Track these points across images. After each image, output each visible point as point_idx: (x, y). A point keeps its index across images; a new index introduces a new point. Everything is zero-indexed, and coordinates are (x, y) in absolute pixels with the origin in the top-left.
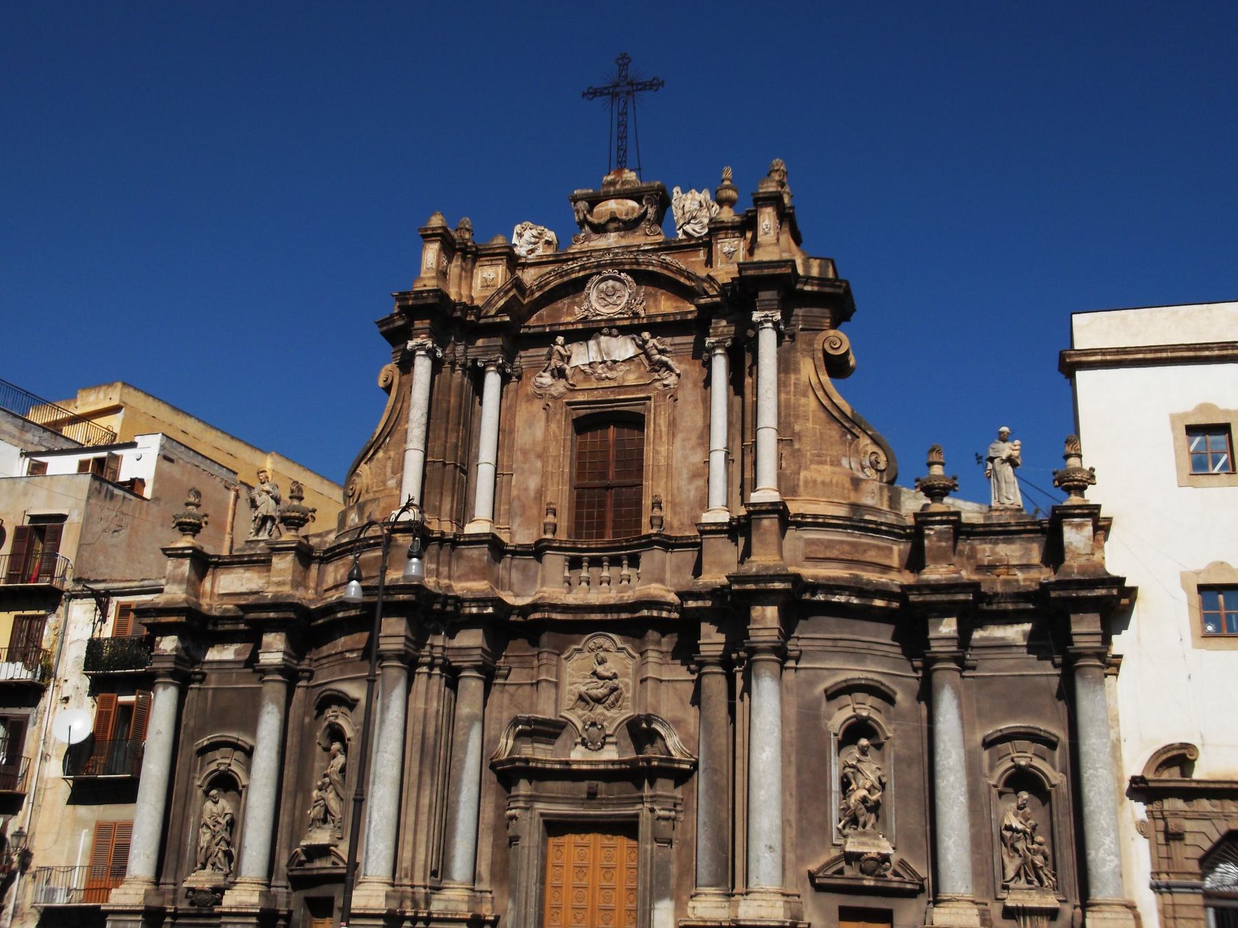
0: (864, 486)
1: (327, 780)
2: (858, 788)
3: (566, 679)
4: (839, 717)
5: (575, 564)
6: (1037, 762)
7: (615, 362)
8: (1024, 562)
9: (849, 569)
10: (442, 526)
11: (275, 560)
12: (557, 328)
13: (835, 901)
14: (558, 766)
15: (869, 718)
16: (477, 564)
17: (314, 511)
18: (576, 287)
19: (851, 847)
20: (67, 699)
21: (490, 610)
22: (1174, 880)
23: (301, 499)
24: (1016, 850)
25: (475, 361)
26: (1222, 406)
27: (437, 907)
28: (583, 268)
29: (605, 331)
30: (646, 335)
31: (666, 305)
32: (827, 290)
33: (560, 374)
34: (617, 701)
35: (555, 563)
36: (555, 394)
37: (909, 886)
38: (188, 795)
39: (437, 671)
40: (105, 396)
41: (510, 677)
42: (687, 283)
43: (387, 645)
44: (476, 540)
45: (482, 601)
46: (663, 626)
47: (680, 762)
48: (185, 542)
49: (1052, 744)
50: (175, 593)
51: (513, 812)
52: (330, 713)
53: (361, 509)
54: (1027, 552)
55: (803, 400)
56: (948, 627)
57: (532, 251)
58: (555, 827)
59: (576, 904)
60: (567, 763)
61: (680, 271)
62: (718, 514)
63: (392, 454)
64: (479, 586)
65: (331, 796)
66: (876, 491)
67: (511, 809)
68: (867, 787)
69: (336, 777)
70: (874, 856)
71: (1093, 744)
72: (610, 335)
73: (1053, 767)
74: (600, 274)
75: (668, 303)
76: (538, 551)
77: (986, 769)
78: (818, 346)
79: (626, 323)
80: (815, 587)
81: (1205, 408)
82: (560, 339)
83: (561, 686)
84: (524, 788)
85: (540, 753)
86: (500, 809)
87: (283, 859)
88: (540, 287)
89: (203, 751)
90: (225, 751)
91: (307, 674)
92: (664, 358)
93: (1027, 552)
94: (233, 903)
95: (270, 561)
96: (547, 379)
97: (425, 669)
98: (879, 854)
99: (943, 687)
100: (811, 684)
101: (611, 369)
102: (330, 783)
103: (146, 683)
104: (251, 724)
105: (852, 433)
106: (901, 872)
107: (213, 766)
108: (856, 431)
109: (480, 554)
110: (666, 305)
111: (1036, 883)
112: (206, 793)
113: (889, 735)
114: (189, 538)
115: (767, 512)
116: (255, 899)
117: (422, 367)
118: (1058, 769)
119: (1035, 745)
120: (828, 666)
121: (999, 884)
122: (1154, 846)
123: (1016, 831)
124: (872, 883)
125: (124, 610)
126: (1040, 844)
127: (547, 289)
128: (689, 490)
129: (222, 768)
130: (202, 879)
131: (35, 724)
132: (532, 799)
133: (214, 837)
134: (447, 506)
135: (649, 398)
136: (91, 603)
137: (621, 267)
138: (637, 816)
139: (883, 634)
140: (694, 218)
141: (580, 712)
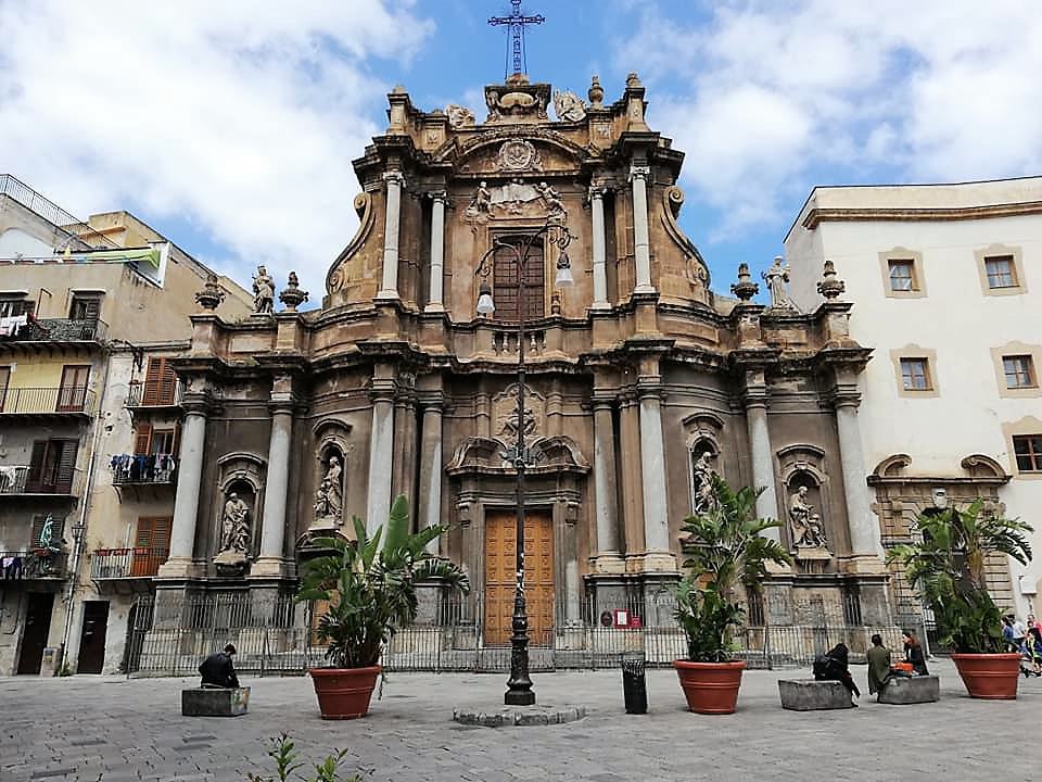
0: (696, 288)
1: (329, 483)
3: (496, 415)
4: (692, 439)
5: (499, 337)
6: (811, 468)
7: (521, 202)
8: (797, 341)
10: (411, 305)
11: (280, 326)
15: (708, 439)
17: (307, 293)
18: (493, 149)
20: (110, 428)
21: (448, 365)
22: (896, 540)
23: (297, 285)
25: (426, 194)
26: (909, 248)
28: (498, 136)
29: (515, 180)
30: (544, 184)
31: (555, 166)
32: (672, 158)
33: (483, 208)
35: (486, 337)
36: (481, 222)
38: (214, 497)
40: (112, 221)
41: (456, 413)
42: (572, 151)
43: (276, 397)
44: (434, 317)
46: (564, 380)
47: (581, 468)
48: (207, 312)
49: (819, 456)
50: (202, 349)
51: (464, 504)
52: (328, 438)
53: (345, 293)
54: (798, 336)
55: (658, 231)
56: (759, 381)
57: (459, 124)
58: (492, 513)
60: (502, 470)
61: (566, 143)
62: (601, 303)
65: (331, 495)
72: (518, 183)
74: (510, 140)
76: (473, 328)
80: (677, 351)
81: (898, 250)
82: (484, 184)
84: (470, 487)
85: (481, 464)
86: (453, 503)
88: (468, 148)
89: (225, 466)
90: (242, 465)
91: (305, 410)
92: (557, 201)
93: (798, 336)
96: (474, 211)
101: (519, 207)
103: (179, 415)
105: (688, 255)
107: (233, 476)
109: (438, 327)
110: (555, 166)
111: (814, 544)
112: (227, 495)
113: (720, 450)
115: (648, 300)
116: (277, 569)
117: (394, 192)
119: (809, 457)
122: (882, 519)
123: (802, 511)
125: (155, 363)
126: (817, 519)
128: (575, 290)
129: (240, 477)
130: (229, 557)
131: (84, 446)
132: (476, 495)
136: (130, 358)
138: (552, 505)
139: (711, 388)
141: (507, 437)
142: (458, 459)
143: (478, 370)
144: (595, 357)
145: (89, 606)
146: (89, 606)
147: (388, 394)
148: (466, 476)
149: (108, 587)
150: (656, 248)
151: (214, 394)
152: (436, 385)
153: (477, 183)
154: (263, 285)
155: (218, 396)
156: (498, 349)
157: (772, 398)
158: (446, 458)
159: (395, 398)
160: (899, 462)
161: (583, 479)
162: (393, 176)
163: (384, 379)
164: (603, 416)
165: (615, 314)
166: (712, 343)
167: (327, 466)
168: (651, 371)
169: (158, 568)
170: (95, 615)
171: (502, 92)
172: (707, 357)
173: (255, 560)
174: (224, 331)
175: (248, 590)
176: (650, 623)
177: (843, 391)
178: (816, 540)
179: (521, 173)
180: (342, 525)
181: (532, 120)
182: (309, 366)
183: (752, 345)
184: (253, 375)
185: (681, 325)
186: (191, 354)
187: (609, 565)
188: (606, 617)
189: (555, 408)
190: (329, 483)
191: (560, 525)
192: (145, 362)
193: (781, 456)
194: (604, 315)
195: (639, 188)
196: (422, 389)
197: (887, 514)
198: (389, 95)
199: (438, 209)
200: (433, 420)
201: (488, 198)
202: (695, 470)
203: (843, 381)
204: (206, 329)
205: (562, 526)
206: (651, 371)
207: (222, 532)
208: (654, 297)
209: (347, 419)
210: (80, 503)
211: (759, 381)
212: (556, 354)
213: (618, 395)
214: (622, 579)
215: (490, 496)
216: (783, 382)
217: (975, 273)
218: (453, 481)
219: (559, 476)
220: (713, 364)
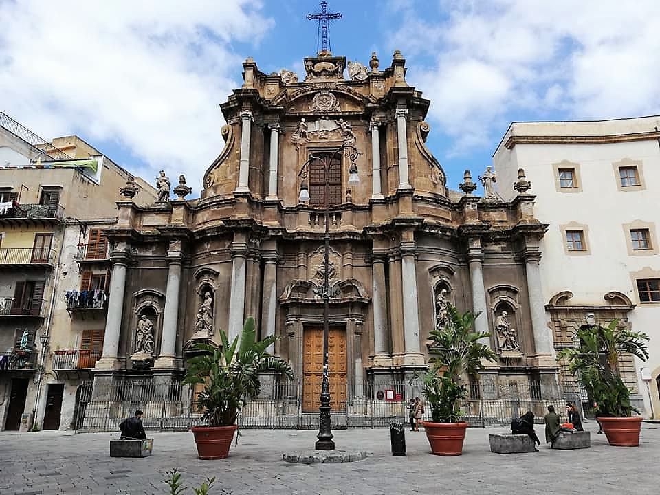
1: (204, 309)
4: (434, 281)
5: (313, 216)
6: (510, 300)
10: (257, 196)
12: (301, 115)
14: (310, 302)
15: (445, 281)
16: (272, 215)
17: (191, 188)
21: (280, 234)
24: (504, 335)
28: (312, 89)
29: (323, 117)
30: (341, 120)
31: (348, 108)
33: (303, 134)
34: (334, 274)
35: (304, 216)
44: (271, 204)
45: (278, 230)
47: (364, 300)
49: (515, 292)
50: (124, 224)
52: (204, 280)
53: (215, 188)
56: (477, 244)
57: (288, 81)
58: (308, 328)
59: (318, 362)
61: (356, 94)
62: (377, 195)
63: (230, 164)
64: (275, 224)
65: (206, 316)
66: (468, 180)
69: (209, 308)
71: (534, 291)
72: (325, 119)
73: (516, 301)
75: (350, 107)
79: (333, 114)
80: (425, 226)
81: (565, 162)
82: (303, 120)
83: (309, 268)
84: (294, 312)
85: (301, 297)
87: (181, 347)
89: (138, 298)
92: (349, 131)
94: (159, 366)
95: (171, 211)
96: (297, 137)
97: (252, 259)
99: (475, 269)
100: (424, 266)
101: (326, 135)
102: (206, 310)
104: (164, 286)
107: (143, 304)
108: (433, 164)
109: (274, 210)
110: (348, 108)
114: (129, 199)
116: (171, 363)
117: (246, 125)
119: (508, 293)
121: (497, 348)
123: (504, 327)
125: (94, 232)
126: (513, 332)
127: (296, 97)
130: (140, 356)
131: (49, 285)
133: (145, 336)
134: (258, 188)
136: (77, 229)
139: (448, 250)
140: (359, 72)
142: (287, 294)
143: (299, 237)
144: (373, 229)
145: (51, 386)
146: (51, 386)
147: (243, 252)
148: (292, 305)
150: (412, 161)
152: (273, 247)
153: (298, 119)
154: (164, 183)
155: (134, 253)
156: (312, 224)
157: (485, 256)
159: (247, 255)
160: (565, 296)
161: (365, 306)
162: (246, 114)
163: (240, 243)
164: (379, 267)
165: (386, 202)
166: (447, 221)
167: (203, 298)
168: (409, 239)
171: (315, 62)
172: (444, 229)
173: (157, 358)
174: (138, 212)
177: (530, 251)
178: (513, 346)
179: (327, 113)
181: (334, 80)
182: (191, 234)
183: (473, 222)
184: (157, 240)
185: (428, 209)
186: (117, 227)
187: (382, 361)
189: (347, 262)
190: (204, 309)
191: (351, 336)
192: (88, 232)
193: (491, 292)
194: (379, 202)
195: (402, 122)
197: (558, 329)
198: (243, 63)
199: (274, 136)
200: (271, 269)
201: (306, 128)
202: (437, 301)
203: (530, 245)
204: (126, 210)
206: (409, 239)
208: (411, 192)
209: (216, 268)
211: (477, 244)
212: (349, 227)
213: (388, 254)
214: (390, 370)
217: (613, 177)
218: (284, 308)
219: (351, 305)
220: (448, 234)
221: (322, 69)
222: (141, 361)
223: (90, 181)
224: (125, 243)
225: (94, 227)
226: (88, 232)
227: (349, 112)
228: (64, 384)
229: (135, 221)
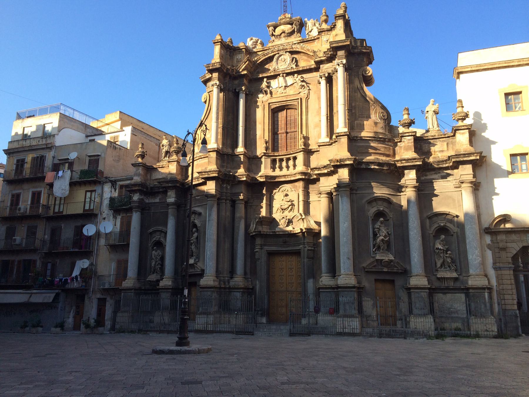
2: (380, 236)
9: (375, 156)
13: (373, 277)
19: (378, 257)
20: (104, 219)
25: (235, 89)
27: (232, 284)
37: (400, 271)
39: (228, 202)
51: (257, 250)
55: (356, 94)
67: (256, 249)
68: (383, 235)
69: (195, 240)
70: (387, 260)
73: (454, 226)
74: (279, 53)
77: (428, 227)
78: (360, 73)
79: (289, 71)
89: (151, 233)
94: (163, 285)
98: (389, 259)
104: (166, 225)
106: (397, 266)
107: (154, 239)
112: (153, 248)
116: (170, 283)
118: (456, 226)
120: (367, 192)
123: (441, 249)
124: (386, 270)
130: (153, 277)
135: (298, 99)
137: (286, 51)
145: (99, 299)
146: (99, 299)
149: (106, 291)
150: (353, 104)
151: (145, 200)
155: (147, 201)
156: (274, 168)
158: (247, 227)
169: (122, 283)
170: (102, 303)
175: (159, 293)
176: (341, 312)
178: (449, 267)
179: (284, 70)
180: (198, 261)
184: (161, 190)
186: (132, 182)
187: (325, 280)
188: (316, 308)
192: (117, 187)
196: (234, 192)
197: (497, 250)
202: (374, 229)
205: (305, 260)
207: (151, 265)
210: (94, 253)
215: (270, 246)
216: (432, 174)
221: (281, 32)
222: (153, 281)
223: (121, 148)
224: (138, 194)
225: (121, 183)
226: (117, 187)
227: (303, 67)
228: (106, 298)
229: (146, 176)
